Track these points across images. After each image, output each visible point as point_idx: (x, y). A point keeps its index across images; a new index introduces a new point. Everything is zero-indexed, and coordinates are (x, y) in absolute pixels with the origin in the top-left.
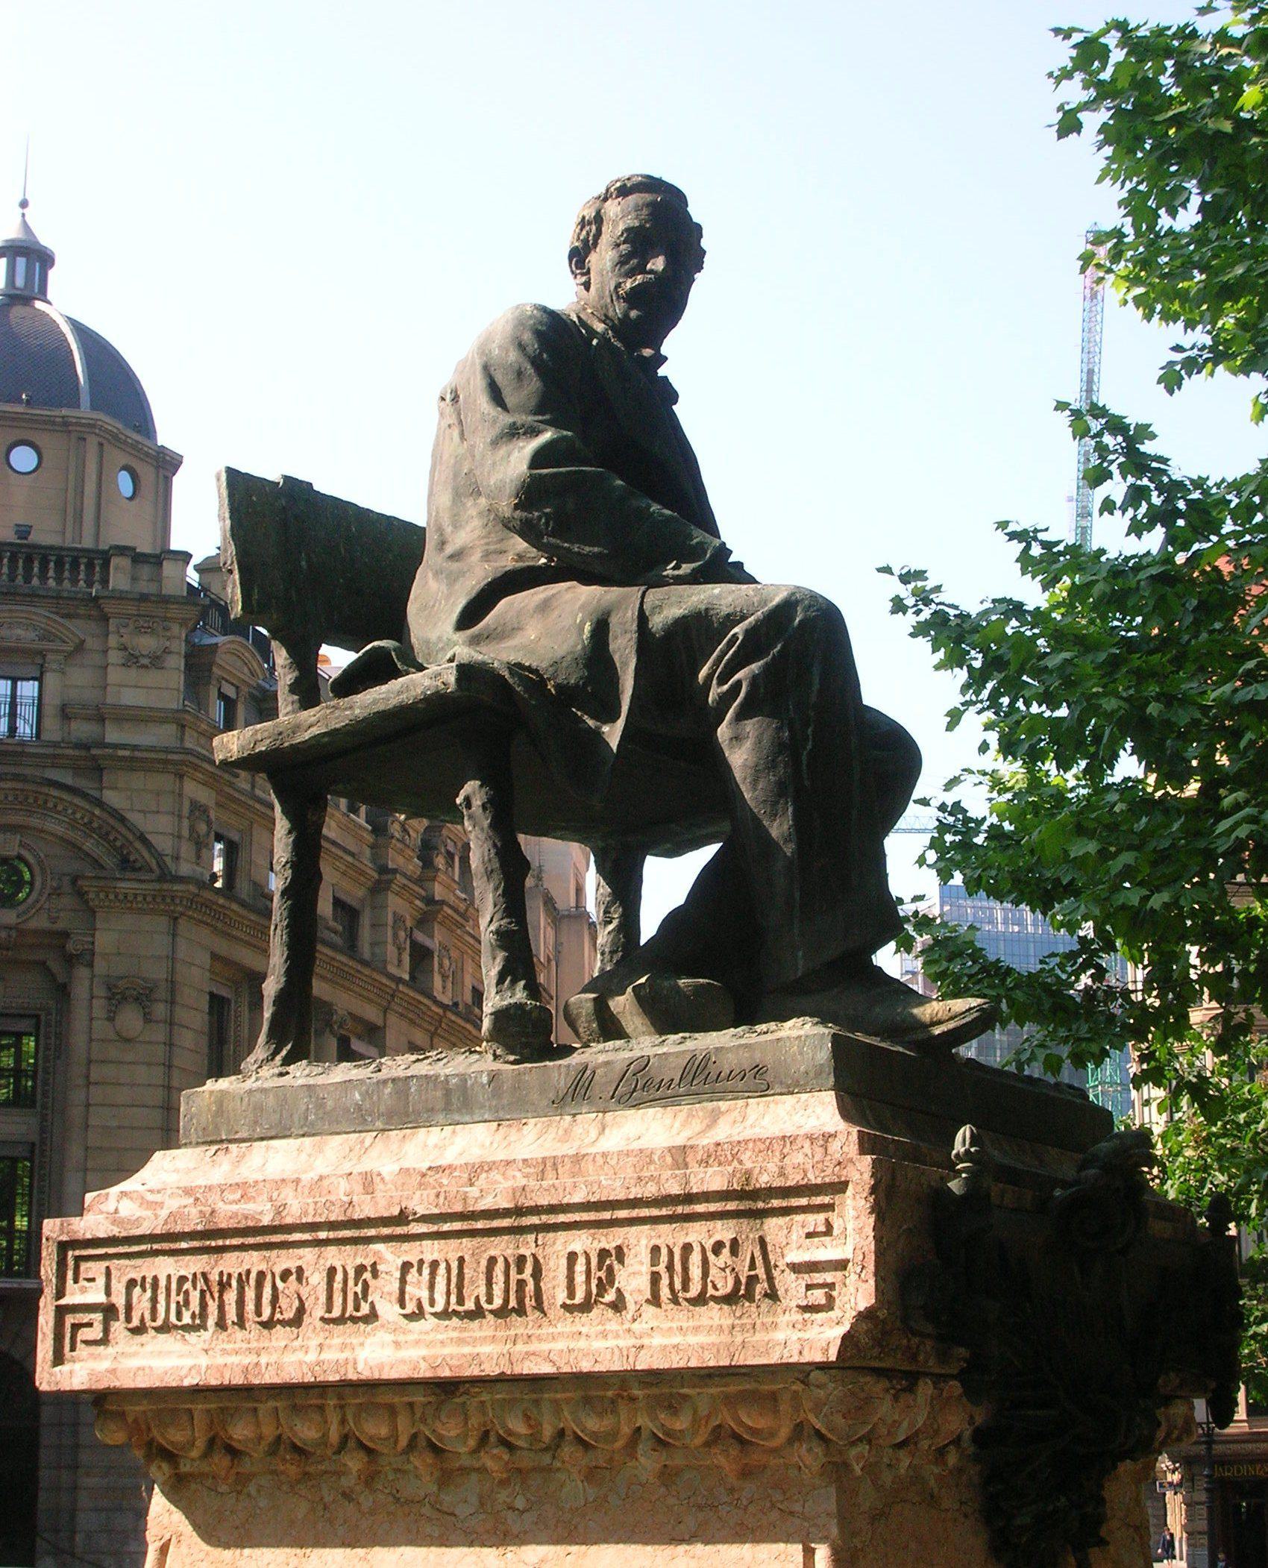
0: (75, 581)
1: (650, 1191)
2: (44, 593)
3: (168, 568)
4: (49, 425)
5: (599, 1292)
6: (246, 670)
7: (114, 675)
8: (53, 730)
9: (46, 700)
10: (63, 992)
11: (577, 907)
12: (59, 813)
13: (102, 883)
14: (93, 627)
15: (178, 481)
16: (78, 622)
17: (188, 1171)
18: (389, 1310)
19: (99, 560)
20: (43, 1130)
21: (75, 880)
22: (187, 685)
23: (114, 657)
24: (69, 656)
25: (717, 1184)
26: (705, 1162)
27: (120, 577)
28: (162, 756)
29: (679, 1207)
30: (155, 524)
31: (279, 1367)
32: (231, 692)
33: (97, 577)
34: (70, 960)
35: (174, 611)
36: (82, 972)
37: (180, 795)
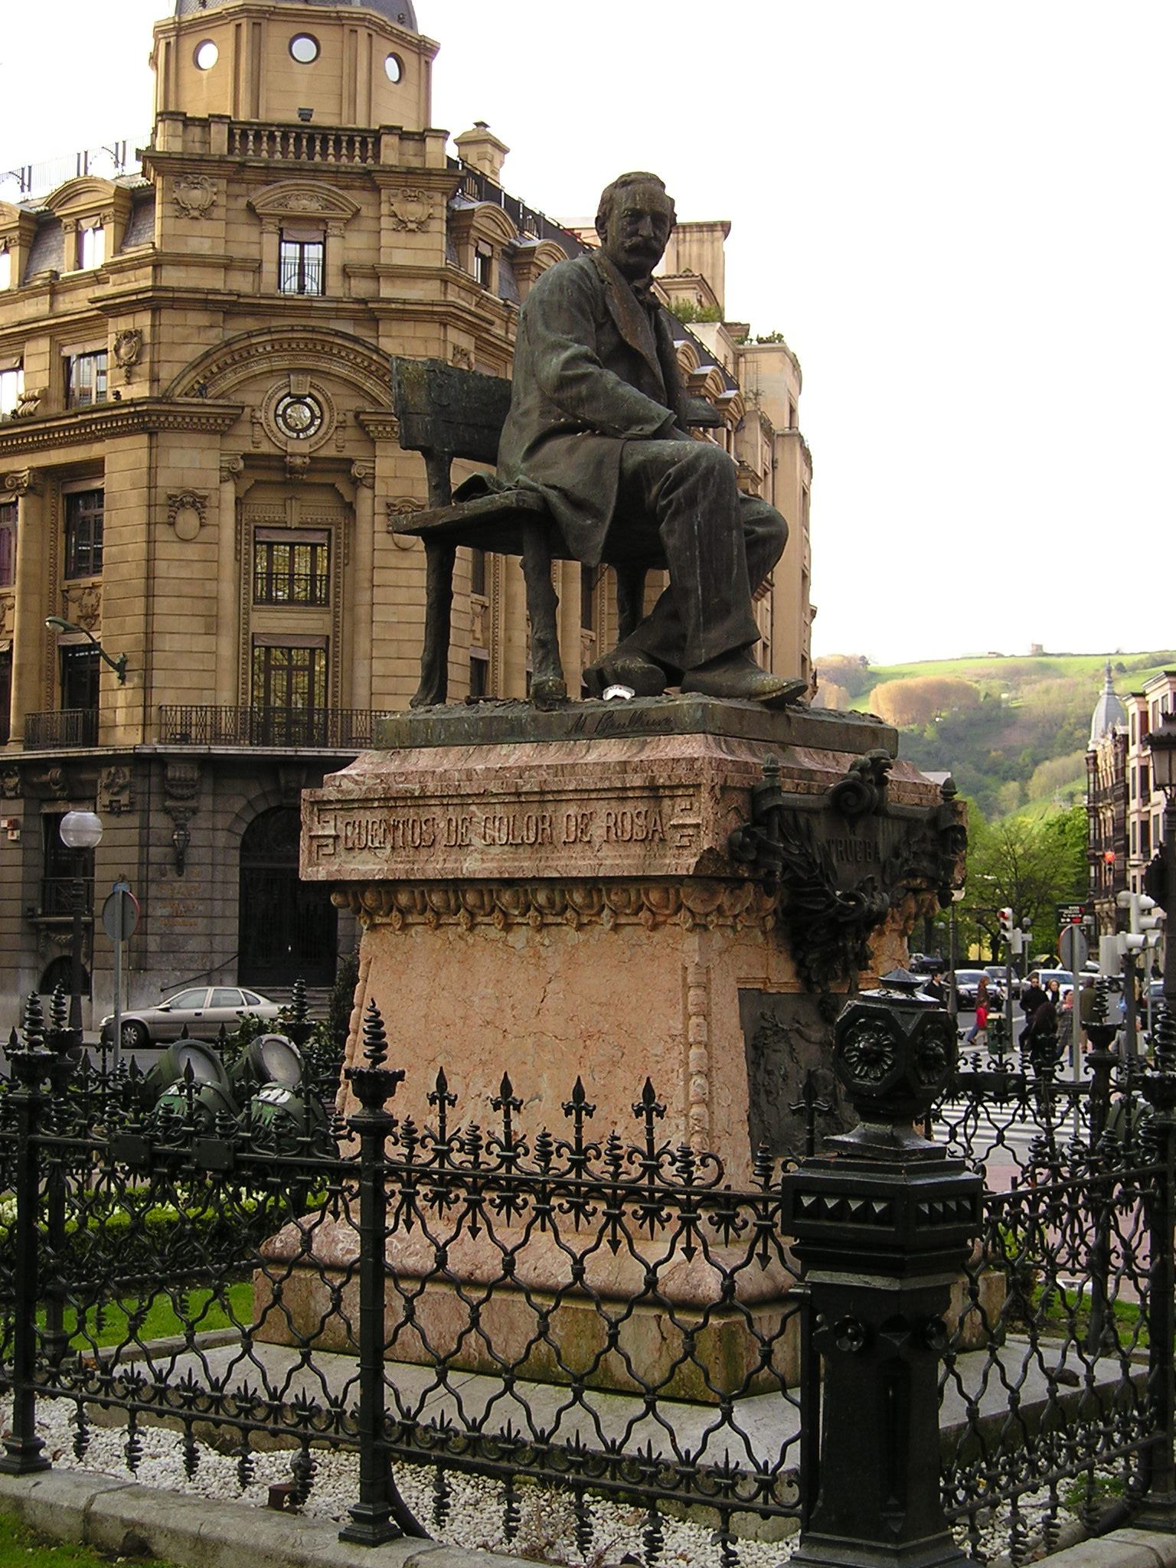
0: (351, 157)
1: (606, 785)
2: (324, 168)
3: (431, 144)
4: (325, 18)
5: (581, 838)
6: (499, 232)
7: (387, 238)
8: (335, 287)
9: (329, 261)
10: (350, 509)
11: (790, 428)
12: (342, 358)
13: (380, 418)
14: (367, 196)
15: (437, 64)
16: (354, 192)
17: (378, 764)
18: (478, 842)
19: (372, 138)
20: (336, 625)
21: (357, 415)
22: (449, 245)
23: (386, 223)
24: (347, 222)
25: (638, 783)
26: (635, 771)
27: (391, 153)
28: (430, 308)
29: (622, 794)
30: (418, 104)
31: (424, 870)
32: (486, 250)
33: (370, 153)
34: (356, 483)
35: (436, 182)
36: (365, 493)
37: (445, 341)
